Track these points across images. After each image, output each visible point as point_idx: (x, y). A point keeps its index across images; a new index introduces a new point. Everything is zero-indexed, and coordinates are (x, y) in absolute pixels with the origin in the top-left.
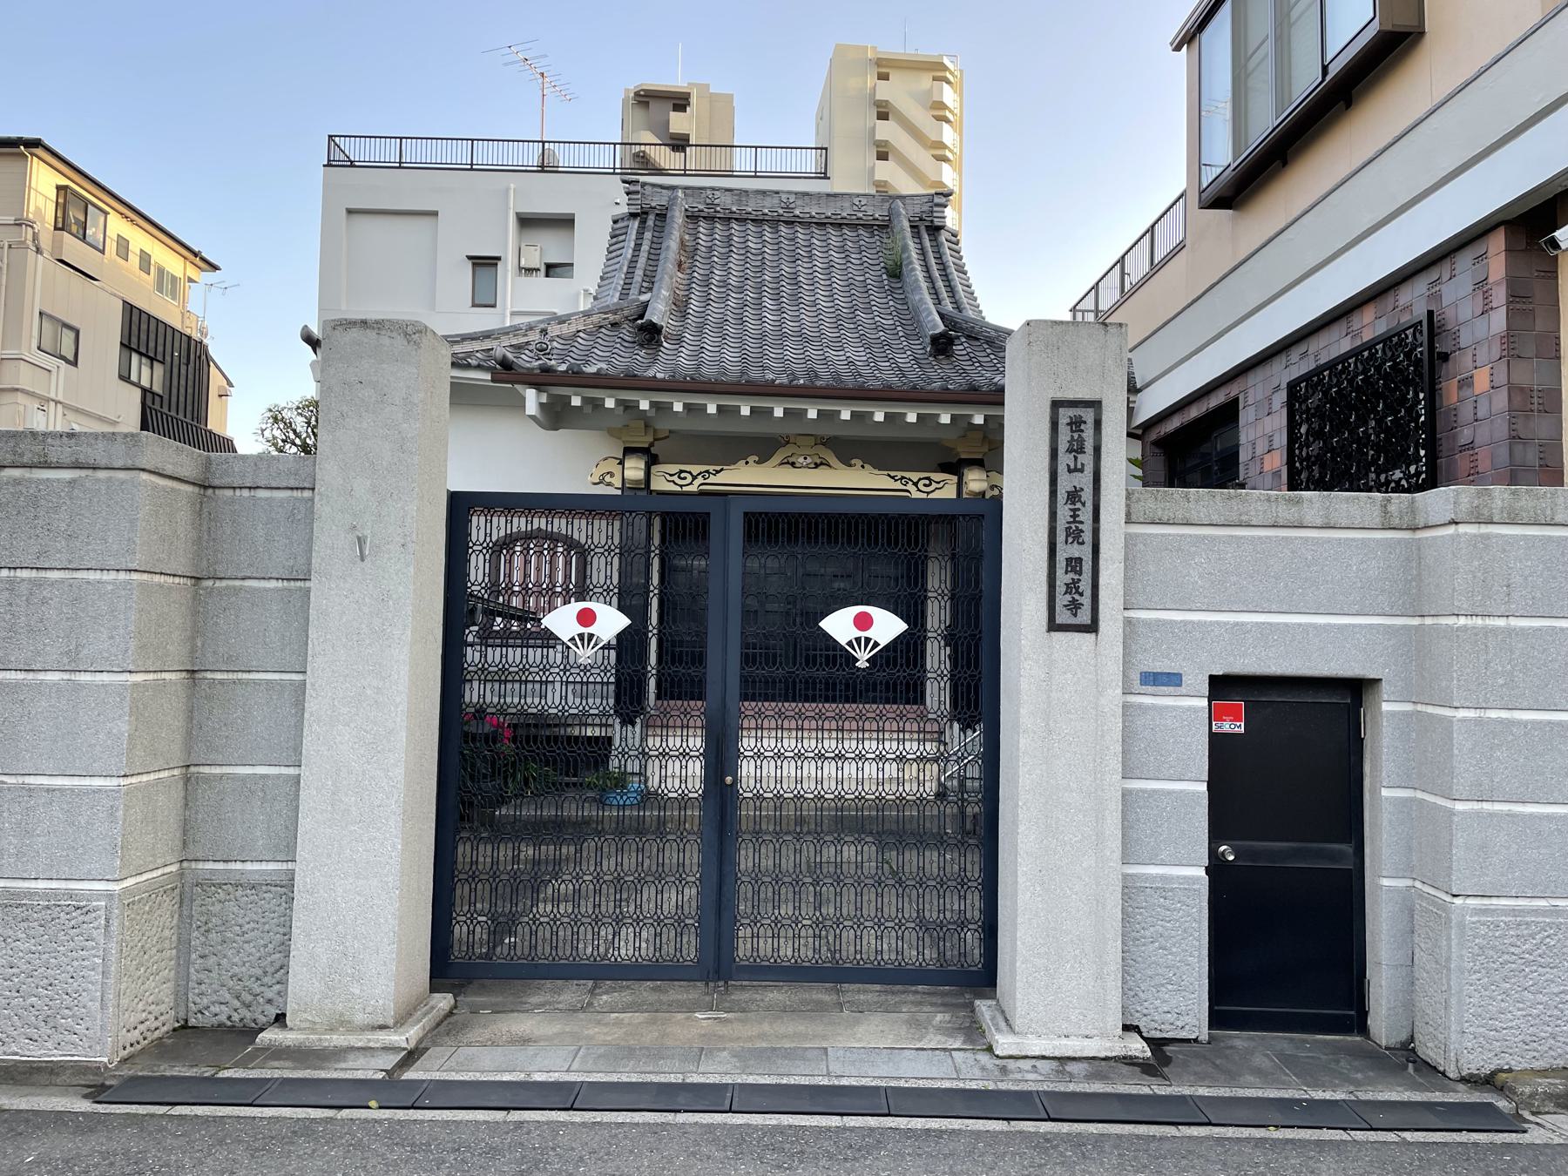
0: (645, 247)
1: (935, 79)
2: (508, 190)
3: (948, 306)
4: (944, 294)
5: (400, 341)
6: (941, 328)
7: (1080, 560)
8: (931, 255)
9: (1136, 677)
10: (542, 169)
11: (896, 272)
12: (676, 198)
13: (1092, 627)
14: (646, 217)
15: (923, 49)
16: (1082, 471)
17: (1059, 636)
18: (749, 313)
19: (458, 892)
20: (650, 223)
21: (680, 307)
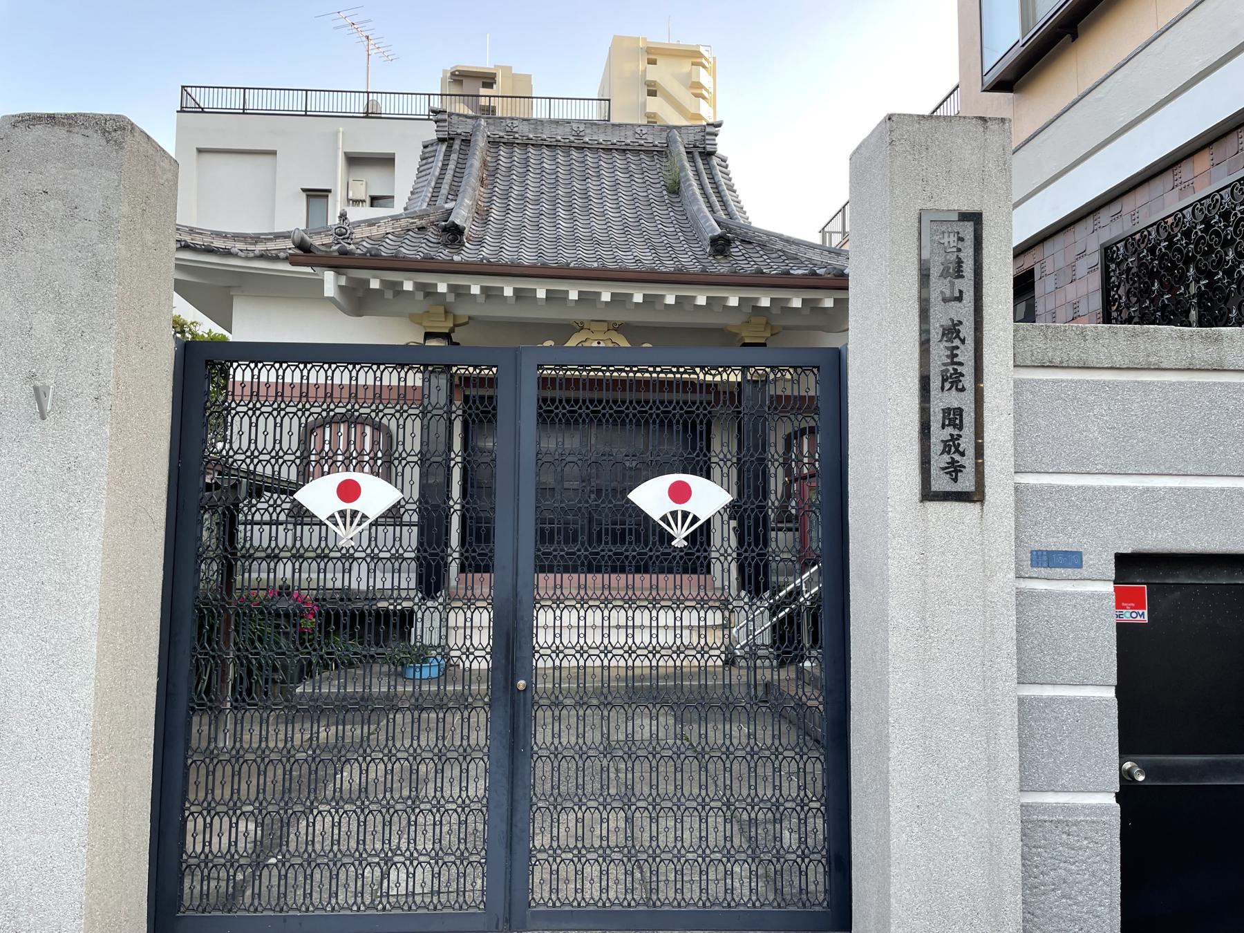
0: (452, 166)
1: (693, 64)
2: (337, 133)
3: (722, 214)
4: (718, 206)
5: (96, 139)
6: (718, 231)
7: (959, 411)
8: (705, 176)
9: (1026, 558)
10: (367, 115)
11: (675, 189)
12: (479, 125)
13: (975, 496)
14: (451, 142)
15: (686, 40)
16: (959, 299)
17: (933, 506)
18: (545, 221)
19: (190, 825)
20: (456, 146)
21: (483, 216)
